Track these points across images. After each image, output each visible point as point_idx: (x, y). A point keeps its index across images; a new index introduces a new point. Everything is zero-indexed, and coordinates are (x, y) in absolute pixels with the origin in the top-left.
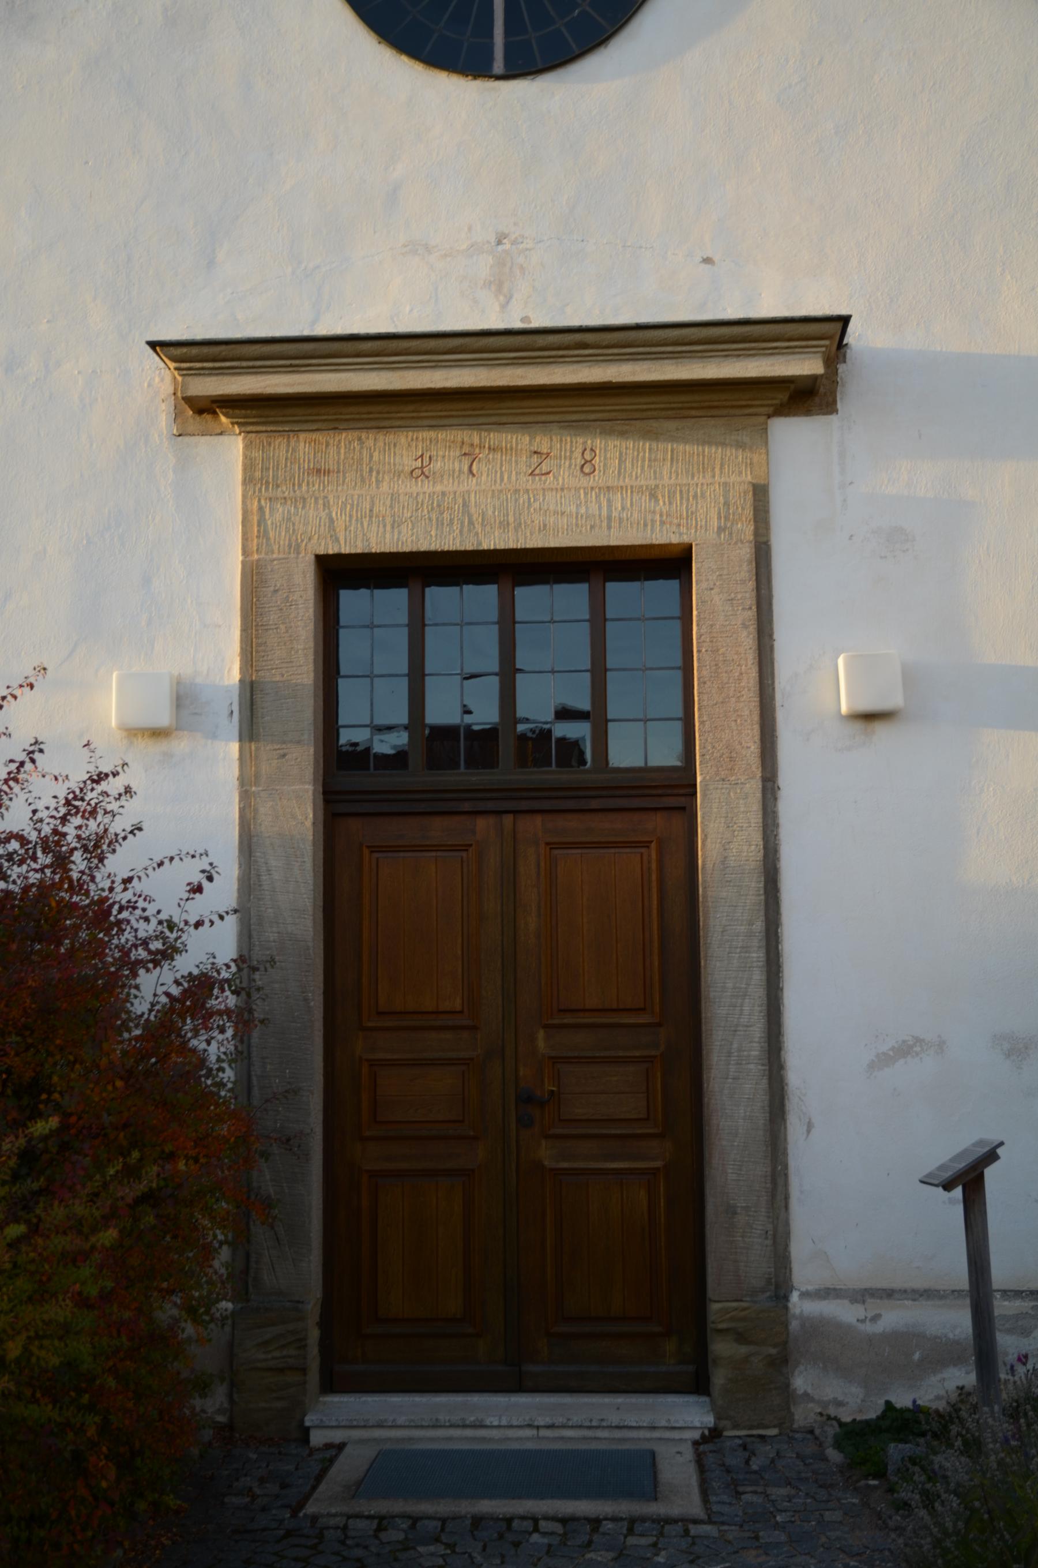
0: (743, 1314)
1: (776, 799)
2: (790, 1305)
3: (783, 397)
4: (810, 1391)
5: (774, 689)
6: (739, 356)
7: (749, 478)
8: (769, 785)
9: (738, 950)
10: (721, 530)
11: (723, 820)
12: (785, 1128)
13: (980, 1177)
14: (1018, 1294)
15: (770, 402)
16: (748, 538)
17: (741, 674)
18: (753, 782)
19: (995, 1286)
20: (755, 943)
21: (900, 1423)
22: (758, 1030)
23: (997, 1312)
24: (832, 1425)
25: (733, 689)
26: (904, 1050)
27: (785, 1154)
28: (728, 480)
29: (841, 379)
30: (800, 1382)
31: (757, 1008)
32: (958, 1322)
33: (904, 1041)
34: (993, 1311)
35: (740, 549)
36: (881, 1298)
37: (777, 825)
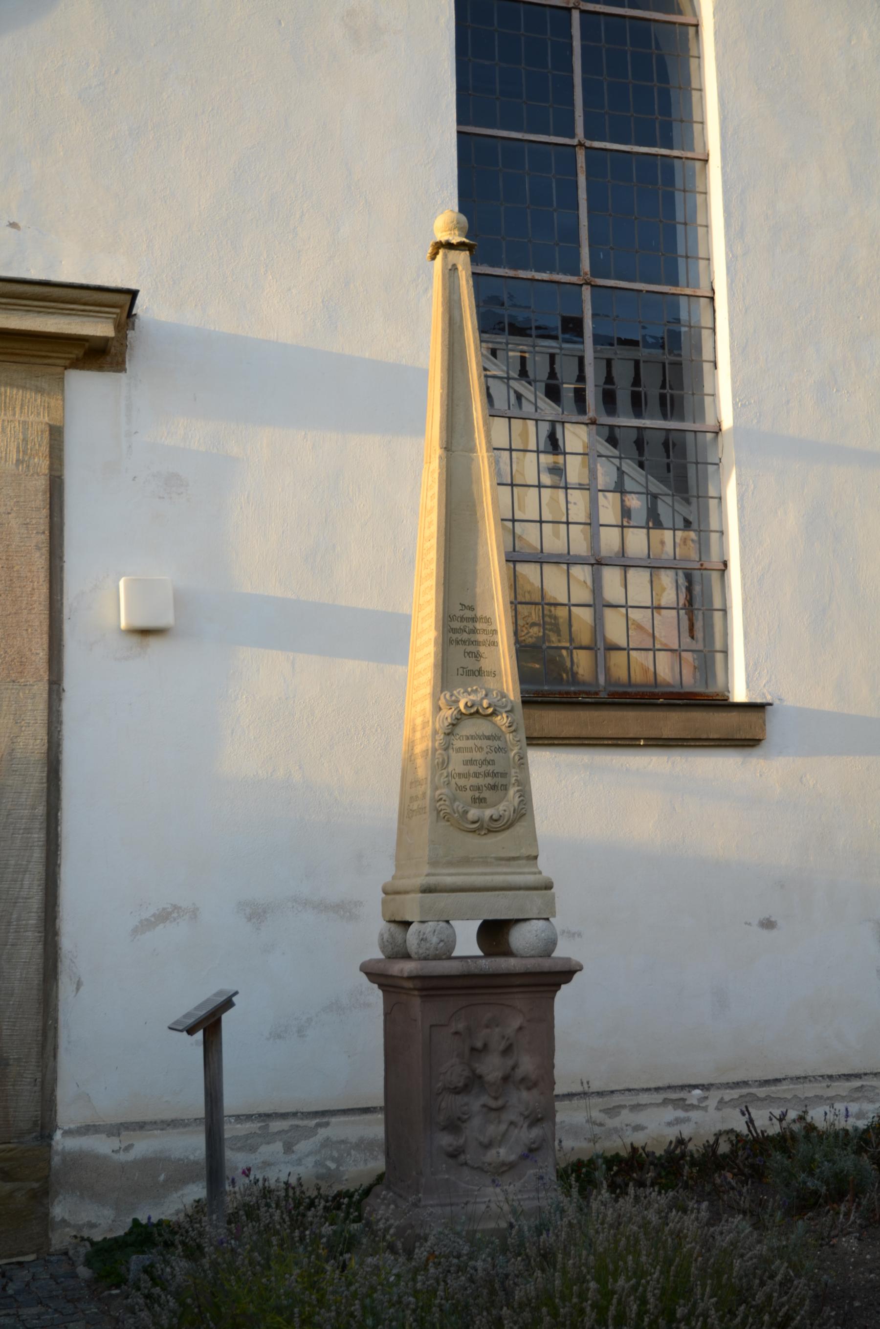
0: (9, 1154)
1: (60, 700)
2: (53, 1143)
3: (78, 352)
4: (66, 1217)
5: (62, 604)
6: (39, 312)
7: (46, 419)
8: (55, 687)
9: (21, 831)
10: (19, 462)
11: (12, 717)
12: (57, 987)
13: (218, 1022)
14: (249, 1117)
15: (67, 356)
16: (43, 471)
17: (33, 589)
18: (40, 684)
19: (226, 1112)
20: (37, 825)
21: (143, 1236)
22: (36, 901)
23: (227, 1135)
24: (84, 1246)
25: (25, 602)
26: (164, 917)
27: (56, 1010)
28: (27, 419)
29: (130, 343)
30: (58, 1211)
31: (36, 882)
32: (192, 1145)
33: (164, 909)
34: (223, 1135)
35: (36, 480)
36: (134, 1130)
37: (60, 723)
